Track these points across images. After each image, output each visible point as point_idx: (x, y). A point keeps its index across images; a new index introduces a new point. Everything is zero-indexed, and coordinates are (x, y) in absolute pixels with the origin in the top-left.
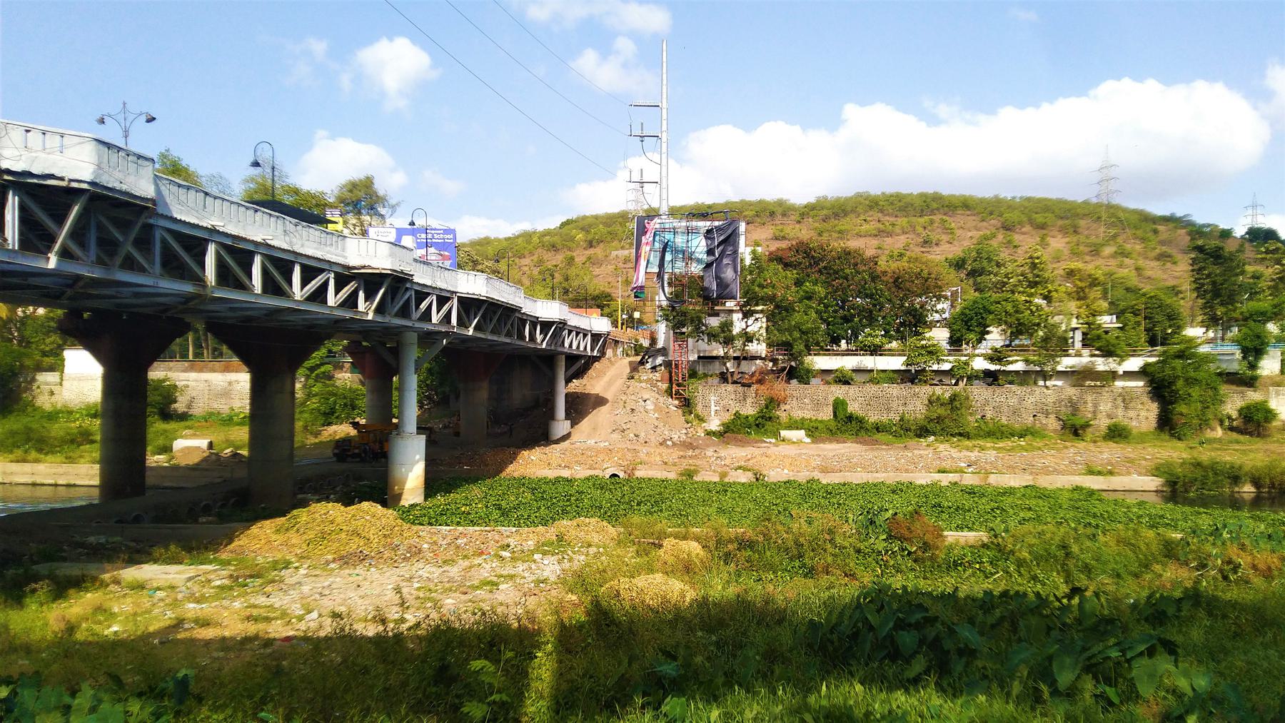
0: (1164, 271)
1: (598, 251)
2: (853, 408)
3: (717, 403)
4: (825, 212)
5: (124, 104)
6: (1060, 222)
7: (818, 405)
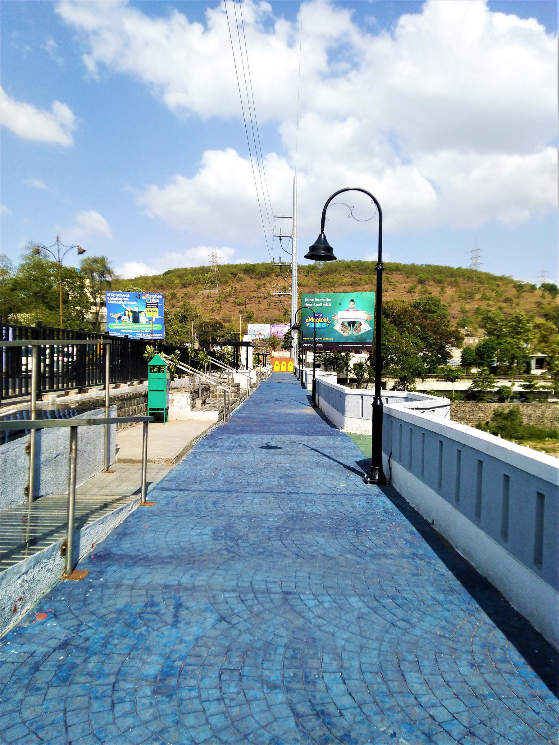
1: (190, 290)
5: (58, 238)
6: (449, 280)
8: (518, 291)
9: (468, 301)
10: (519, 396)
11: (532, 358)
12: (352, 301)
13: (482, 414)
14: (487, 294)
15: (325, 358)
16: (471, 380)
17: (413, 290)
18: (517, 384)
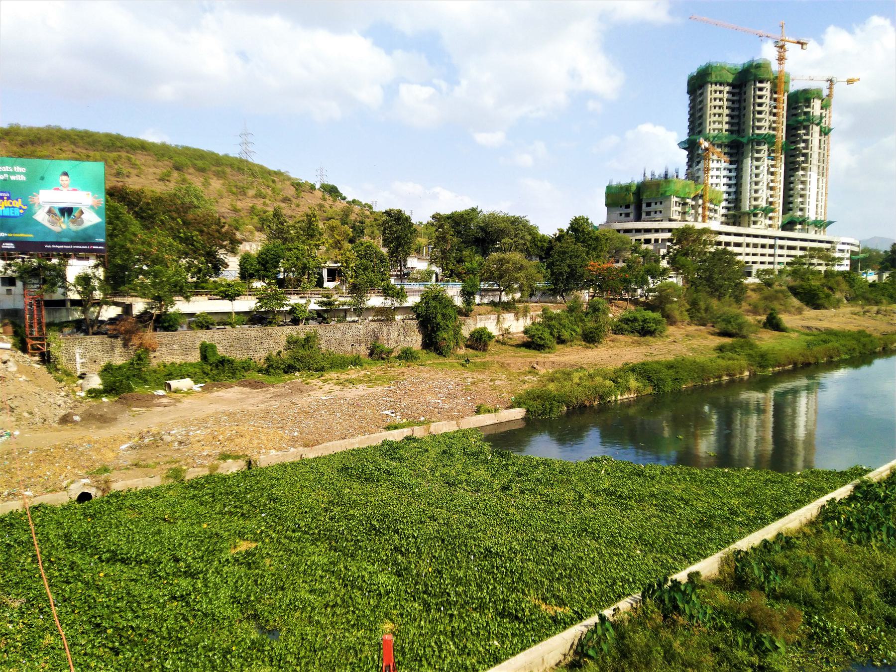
0: (166, 186)
2: (221, 351)
3: (83, 356)
4: (20, 138)
6: (214, 168)
7: (186, 350)
8: (297, 190)
9: (241, 197)
10: (316, 316)
11: (324, 267)
12: (65, 174)
13: (271, 342)
14: (262, 190)
15: (20, 267)
16: (254, 298)
17: (167, 178)
18: (313, 300)
